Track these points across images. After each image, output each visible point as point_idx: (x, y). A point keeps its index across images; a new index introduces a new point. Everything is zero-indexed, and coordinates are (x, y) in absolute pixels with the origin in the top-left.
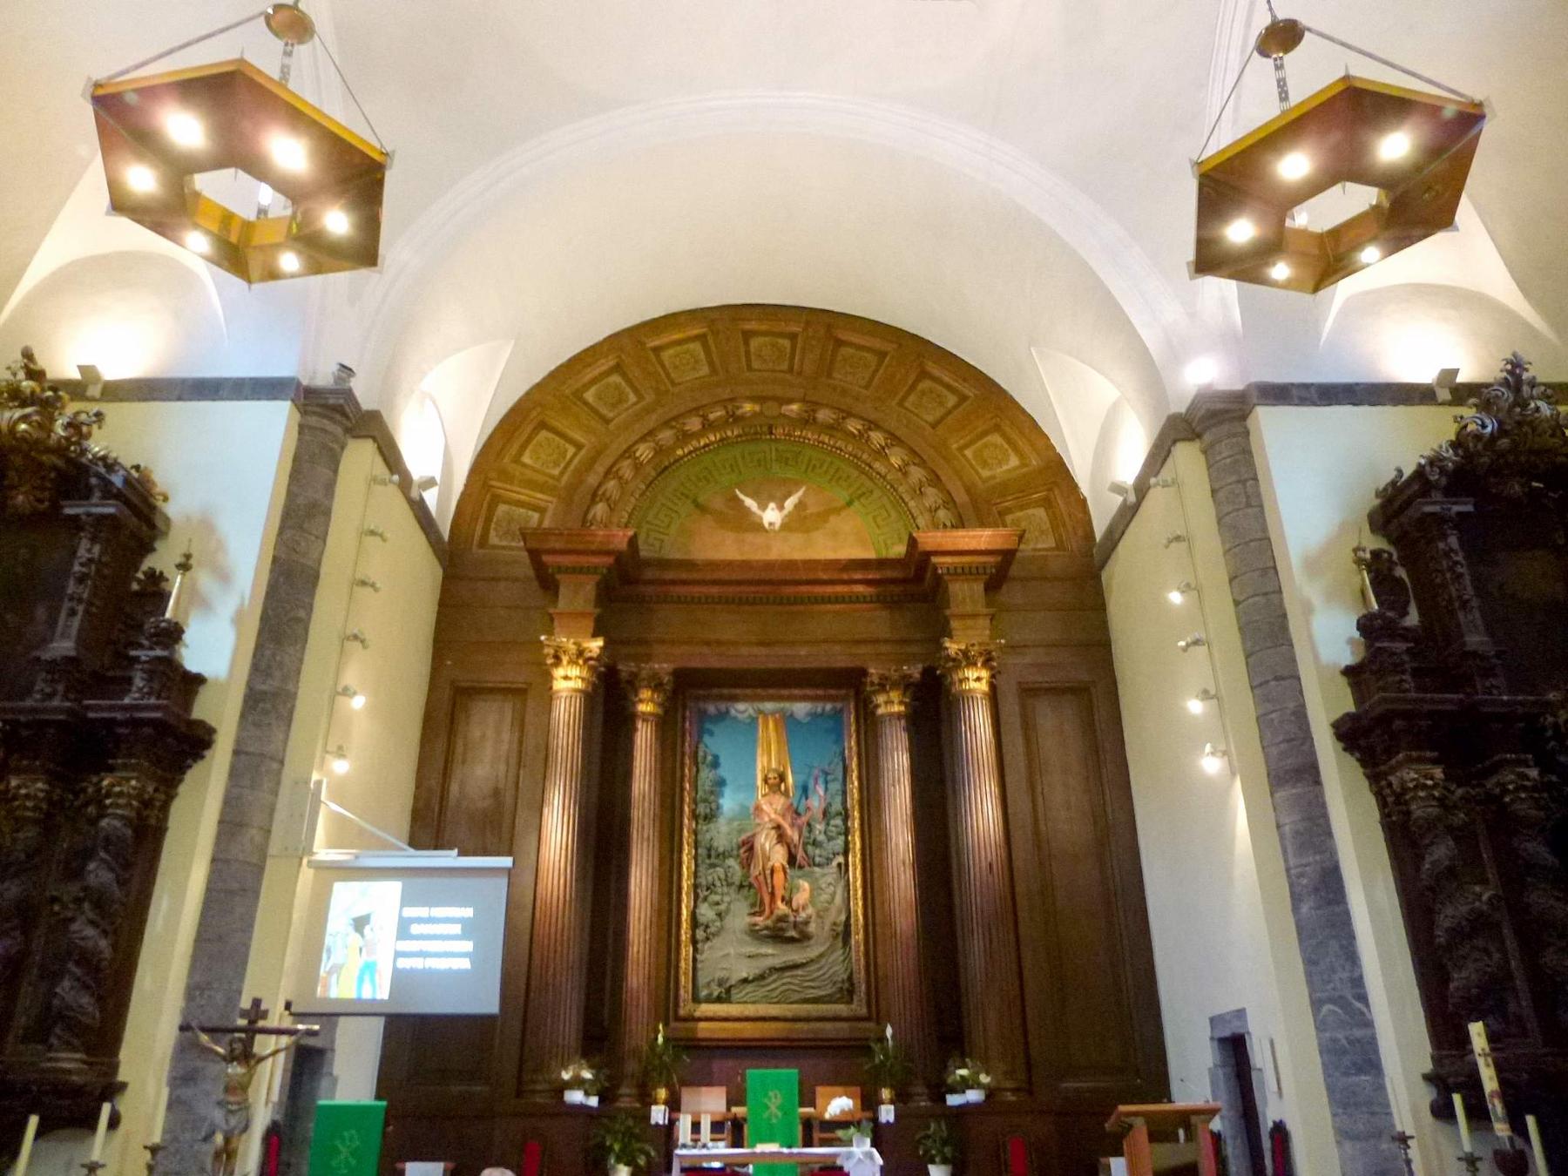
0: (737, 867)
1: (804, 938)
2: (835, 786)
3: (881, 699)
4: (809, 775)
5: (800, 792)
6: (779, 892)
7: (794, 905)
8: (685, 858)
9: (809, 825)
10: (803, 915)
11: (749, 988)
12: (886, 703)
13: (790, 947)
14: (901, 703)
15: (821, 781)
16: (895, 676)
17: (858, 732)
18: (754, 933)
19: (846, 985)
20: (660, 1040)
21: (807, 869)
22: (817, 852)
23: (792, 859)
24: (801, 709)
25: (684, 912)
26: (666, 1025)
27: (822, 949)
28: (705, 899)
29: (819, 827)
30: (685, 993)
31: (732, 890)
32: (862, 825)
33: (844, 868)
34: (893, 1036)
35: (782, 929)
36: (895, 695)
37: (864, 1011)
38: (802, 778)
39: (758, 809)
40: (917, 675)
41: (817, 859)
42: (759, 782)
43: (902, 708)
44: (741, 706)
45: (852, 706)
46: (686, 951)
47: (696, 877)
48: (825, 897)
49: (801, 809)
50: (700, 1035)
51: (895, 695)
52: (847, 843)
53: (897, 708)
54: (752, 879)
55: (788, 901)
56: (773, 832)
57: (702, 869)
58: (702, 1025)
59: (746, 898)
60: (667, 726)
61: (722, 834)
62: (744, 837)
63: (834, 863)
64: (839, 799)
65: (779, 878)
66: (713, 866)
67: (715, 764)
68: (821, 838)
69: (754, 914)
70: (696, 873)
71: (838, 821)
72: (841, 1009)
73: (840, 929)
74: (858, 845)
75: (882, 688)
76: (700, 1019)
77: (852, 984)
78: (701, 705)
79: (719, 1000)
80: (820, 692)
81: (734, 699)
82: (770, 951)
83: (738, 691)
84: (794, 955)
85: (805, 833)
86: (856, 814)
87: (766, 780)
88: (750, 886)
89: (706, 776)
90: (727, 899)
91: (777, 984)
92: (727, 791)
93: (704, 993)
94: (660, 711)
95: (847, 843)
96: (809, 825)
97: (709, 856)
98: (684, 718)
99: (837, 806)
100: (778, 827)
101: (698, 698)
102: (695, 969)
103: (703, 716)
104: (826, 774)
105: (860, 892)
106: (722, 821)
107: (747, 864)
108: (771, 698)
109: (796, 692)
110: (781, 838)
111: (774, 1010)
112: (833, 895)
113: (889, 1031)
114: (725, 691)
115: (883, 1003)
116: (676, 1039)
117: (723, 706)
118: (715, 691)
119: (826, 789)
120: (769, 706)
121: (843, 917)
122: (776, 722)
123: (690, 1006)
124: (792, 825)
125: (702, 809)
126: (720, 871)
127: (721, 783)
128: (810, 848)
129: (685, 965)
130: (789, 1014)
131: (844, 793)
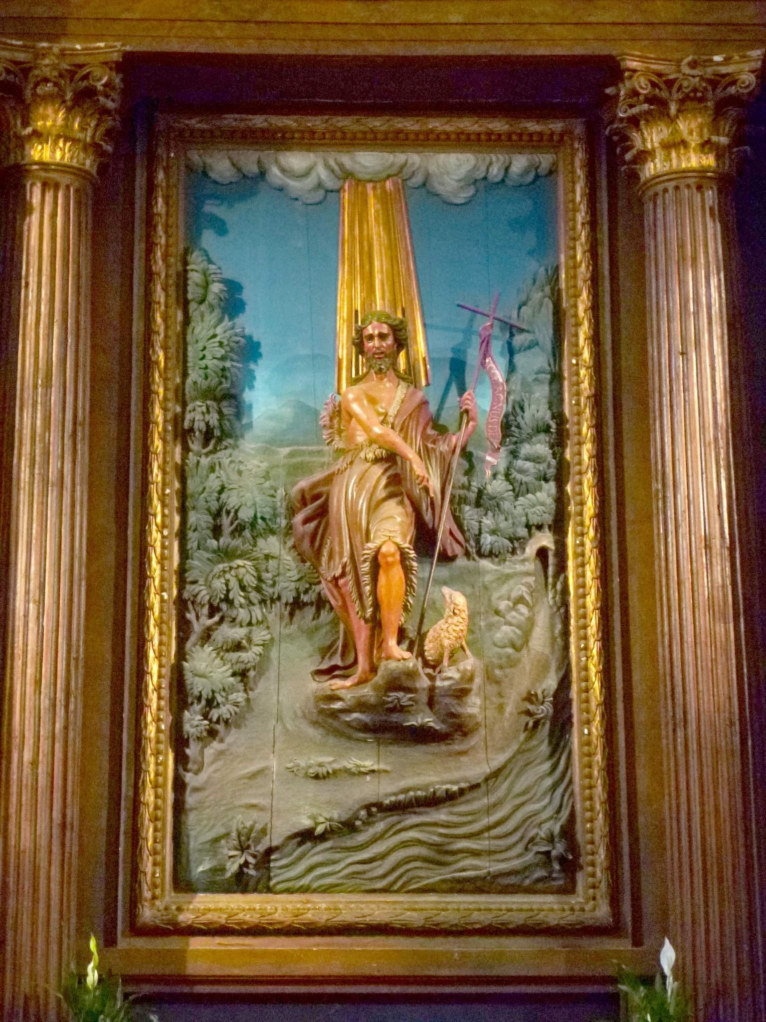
0: (289, 559)
1: (452, 731)
2: (534, 362)
3: (653, 136)
4: (468, 332)
5: (446, 372)
6: (393, 618)
7: (430, 648)
8: (155, 536)
9: (467, 455)
10: (451, 674)
11: (317, 854)
12: (667, 146)
13: (417, 752)
14: (706, 145)
15: (497, 346)
16: (691, 78)
17: (593, 224)
18: (328, 718)
19: (559, 848)
20: (92, 977)
21: (461, 562)
22: (488, 522)
23: (424, 538)
24: (452, 168)
25: (153, 666)
26: (109, 940)
27: (500, 759)
28: (207, 636)
29: (494, 460)
30: (155, 867)
31: (274, 614)
32: (599, 456)
33: (553, 563)
34: (677, 969)
35: (401, 709)
36: (690, 127)
37: (602, 912)
38: (447, 344)
39: (340, 412)
40: (748, 79)
41: (487, 540)
42: (344, 349)
43: (710, 161)
44: (296, 160)
45: (580, 157)
46: (158, 764)
47: (182, 583)
48: (505, 632)
49: (448, 418)
50: (195, 967)
51: (690, 127)
52: (561, 500)
53: (696, 160)
54: (324, 588)
55: (414, 642)
56: (377, 470)
57: (196, 563)
58: (197, 943)
59: (310, 633)
60: (110, 201)
61: (249, 475)
62: (304, 483)
63: (531, 550)
64: (542, 392)
65: (392, 581)
66: (227, 554)
67: (232, 304)
68: (498, 486)
69: (330, 672)
70: (182, 572)
71: (541, 447)
72: (547, 907)
73: (545, 709)
74: (590, 508)
75: (658, 107)
76: (192, 931)
77: (573, 846)
78: (195, 157)
79: (240, 883)
80: (499, 125)
81: (280, 140)
82: (369, 764)
83: (289, 122)
84: (427, 772)
85: (458, 476)
86: (587, 431)
87: (359, 344)
88: (321, 603)
89: (208, 331)
90: (260, 635)
91: (389, 843)
92: (262, 372)
93: (201, 868)
94: (89, 163)
95: (561, 500)
96: (467, 455)
97: (217, 531)
98: (151, 188)
99: (537, 410)
100: (390, 458)
101: (187, 139)
102: (179, 808)
103: (199, 176)
104: (512, 330)
105: (594, 622)
106: (249, 444)
107: (312, 548)
108: (372, 141)
109: (436, 124)
110: (397, 482)
111: (378, 908)
112: (527, 630)
113: (668, 956)
114: (259, 121)
115: (648, 887)
116: (129, 980)
117: (249, 159)
118: (230, 120)
119: (512, 368)
120: (368, 161)
121: (551, 683)
122: (384, 199)
123: (170, 897)
124: (426, 453)
125: (199, 414)
126: (245, 568)
127: (249, 350)
128: (469, 513)
129: (155, 797)
130: (415, 919)
131: (556, 378)
